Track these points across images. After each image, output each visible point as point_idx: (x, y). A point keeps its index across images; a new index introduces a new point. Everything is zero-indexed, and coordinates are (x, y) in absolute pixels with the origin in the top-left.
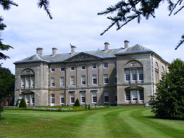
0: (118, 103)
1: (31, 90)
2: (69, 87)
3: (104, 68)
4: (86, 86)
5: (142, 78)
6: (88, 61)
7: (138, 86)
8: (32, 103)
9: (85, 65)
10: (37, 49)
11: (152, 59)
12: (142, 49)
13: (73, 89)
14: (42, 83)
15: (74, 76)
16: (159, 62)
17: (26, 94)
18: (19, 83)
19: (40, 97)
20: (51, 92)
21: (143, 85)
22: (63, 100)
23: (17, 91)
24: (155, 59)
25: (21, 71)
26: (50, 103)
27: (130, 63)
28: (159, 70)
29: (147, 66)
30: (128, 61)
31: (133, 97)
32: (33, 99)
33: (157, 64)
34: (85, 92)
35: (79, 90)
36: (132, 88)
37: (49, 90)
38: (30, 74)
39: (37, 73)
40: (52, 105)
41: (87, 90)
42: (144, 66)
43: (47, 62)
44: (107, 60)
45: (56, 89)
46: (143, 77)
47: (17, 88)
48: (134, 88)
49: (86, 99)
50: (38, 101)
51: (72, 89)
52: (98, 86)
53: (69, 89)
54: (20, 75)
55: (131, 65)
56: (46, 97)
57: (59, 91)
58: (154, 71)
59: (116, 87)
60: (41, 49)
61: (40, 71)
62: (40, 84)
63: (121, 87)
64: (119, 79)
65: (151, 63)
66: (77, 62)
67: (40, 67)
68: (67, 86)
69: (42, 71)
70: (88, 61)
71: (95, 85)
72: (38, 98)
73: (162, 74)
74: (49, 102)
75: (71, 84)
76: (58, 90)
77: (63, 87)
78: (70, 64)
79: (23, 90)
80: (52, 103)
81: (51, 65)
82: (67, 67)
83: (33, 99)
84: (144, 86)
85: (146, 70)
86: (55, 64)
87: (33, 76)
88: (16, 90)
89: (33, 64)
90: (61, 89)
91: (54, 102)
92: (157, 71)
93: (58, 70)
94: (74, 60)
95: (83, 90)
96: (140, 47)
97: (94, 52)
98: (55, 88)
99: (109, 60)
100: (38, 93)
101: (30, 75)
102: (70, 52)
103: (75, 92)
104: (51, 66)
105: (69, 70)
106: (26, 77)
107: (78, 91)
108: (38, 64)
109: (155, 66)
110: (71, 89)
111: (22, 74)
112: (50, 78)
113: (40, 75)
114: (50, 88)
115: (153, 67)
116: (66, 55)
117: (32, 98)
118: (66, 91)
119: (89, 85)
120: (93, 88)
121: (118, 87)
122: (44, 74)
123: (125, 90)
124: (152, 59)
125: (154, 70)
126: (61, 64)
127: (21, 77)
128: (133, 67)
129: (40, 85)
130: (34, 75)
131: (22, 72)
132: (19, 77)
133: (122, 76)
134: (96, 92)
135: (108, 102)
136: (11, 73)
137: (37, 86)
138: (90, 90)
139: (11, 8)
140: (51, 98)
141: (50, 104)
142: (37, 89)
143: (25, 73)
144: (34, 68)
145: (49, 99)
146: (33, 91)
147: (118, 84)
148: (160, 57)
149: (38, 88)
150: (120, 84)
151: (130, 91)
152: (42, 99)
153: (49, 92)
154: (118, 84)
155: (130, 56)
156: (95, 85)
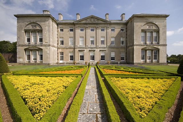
0: (134, 62)
1: (39, 46)
2: (79, 46)
4: (95, 46)
6: (97, 24)
8: (38, 60)
9: (94, 27)
13: (83, 48)
14: (51, 40)
15: (83, 37)
17: (32, 50)
18: (23, 38)
19: (49, 54)
20: (60, 50)
21: (159, 46)
22: (72, 58)
23: (19, 47)
25: (25, 25)
26: (59, 60)
30: (145, 23)
31: (32, 57)
32: (41, 56)
34: (94, 51)
35: (88, 49)
36: (147, 48)
37: (58, 48)
38: (36, 29)
39: (45, 29)
40: (61, 62)
42: (161, 29)
44: (115, 25)
45: (64, 47)
47: (20, 44)
49: (85, 57)
50: (47, 58)
51: (81, 48)
52: (106, 46)
53: (79, 48)
54: (23, 29)
55: (148, 27)
56: (56, 54)
57: (68, 49)
61: (49, 26)
62: (50, 40)
63: (138, 47)
67: (49, 22)
68: (76, 45)
69: (52, 27)
70: (97, 24)
71: (103, 46)
72: (47, 55)
74: (58, 59)
75: (80, 43)
76: (67, 49)
77: (73, 46)
78: (79, 26)
79: (28, 46)
80: (61, 60)
82: (76, 28)
83: (41, 56)
84: (159, 47)
85: (162, 32)
86: (64, 25)
87: (41, 31)
88: (18, 46)
89: (43, 19)
90: (70, 48)
91: (63, 59)
93: (66, 30)
94: (84, 22)
95: (93, 49)
98: (64, 46)
99: (116, 25)
100: (47, 50)
101: (37, 30)
103: (84, 50)
104: (60, 26)
105: (78, 31)
106: (32, 32)
107: (87, 50)
108: (46, 19)
110: (80, 48)
111: (26, 29)
112: (59, 37)
113: (49, 31)
114: (58, 46)
117: (40, 55)
118: (76, 49)
119: (98, 45)
120: (102, 48)
121: (135, 47)
122: (52, 33)
126: (70, 25)
127: (25, 32)
128: (149, 29)
129: (49, 41)
130: (42, 30)
131: (26, 26)
132: (23, 31)
134: (105, 51)
135: (114, 60)
136: (15, 87)
137: (46, 42)
138: (99, 49)
140: (60, 55)
141: (58, 61)
142: (45, 46)
143: (30, 27)
144: (42, 24)
145: (58, 57)
146: (41, 47)
147: (135, 44)
149: (46, 45)
150: (137, 44)
151: (146, 51)
152: (51, 56)
153: (57, 50)
156: (103, 46)
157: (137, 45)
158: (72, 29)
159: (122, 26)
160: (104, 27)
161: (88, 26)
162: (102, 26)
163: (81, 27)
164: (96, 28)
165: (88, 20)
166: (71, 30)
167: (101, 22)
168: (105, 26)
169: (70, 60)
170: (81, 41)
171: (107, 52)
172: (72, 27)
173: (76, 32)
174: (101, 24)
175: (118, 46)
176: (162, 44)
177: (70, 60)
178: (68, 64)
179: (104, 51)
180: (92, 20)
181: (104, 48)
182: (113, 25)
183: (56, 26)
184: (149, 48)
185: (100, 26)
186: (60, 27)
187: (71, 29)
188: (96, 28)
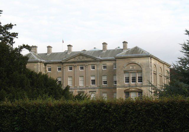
3: (103, 69)
5: (141, 79)
7: (137, 88)
10: (48, 47)
11: (151, 62)
12: (141, 52)
15: (72, 77)
16: (157, 63)
24: (153, 61)
27: (129, 65)
28: (157, 72)
29: (146, 69)
33: (155, 66)
36: (131, 90)
41: (85, 90)
42: (144, 69)
43: (44, 62)
46: (142, 79)
48: (133, 90)
52: (96, 86)
55: (131, 67)
58: (153, 74)
59: (115, 88)
60: (126, 43)
63: (120, 88)
64: (119, 81)
65: (150, 66)
66: (75, 62)
73: (160, 75)
81: (47, 64)
82: (64, 67)
84: (143, 88)
92: (155, 73)
94: (72, 60)
95: (81, 90)
96: (139, 50)
97: (92, 52)
102: (102, 49)
104: (48, 65)
109: (153, 69)
110: (81, 89)
115: (151, 70)
116: (61, 54)
119: (87, 85)
120: (92, 88)
121: (117, 89)
123: (124, 92)
124: (151, 62)
125: (153, 72)
133: (122, 79)
134: (95, 93)
138: (88, 90)
139: (180, 48)
148: (158, 59)
151: (129, 93)
154: (117, 85)
155: (130, 59)
157: (119, 87)
158: (60, 67)
159: (114, 63)
160: (72, 66)
161: (76, 64)
162: (92, 64)
163: (80, 65)
164: (85, 66)
165: (77, 58)
166: (60, 69)
167: (90, 59)
168: (95, 64)
169: (139, 82)
170: (70, 82)
171: (97, 93)
172: (60, 66)
173: (64, 72)
174: (90, 61)
175: (110, 87)
176: (145, 85)
177: (139, 82)
178: (156, 77)
179: (93, 93)
180: (81, 57)
181: (94, 88)
182: (104, 62)
183: (44, 66)
184: (132, 89)
185: (90, 64)
186: (48, 67)
187: (59, 67)
188: (85, 66)
